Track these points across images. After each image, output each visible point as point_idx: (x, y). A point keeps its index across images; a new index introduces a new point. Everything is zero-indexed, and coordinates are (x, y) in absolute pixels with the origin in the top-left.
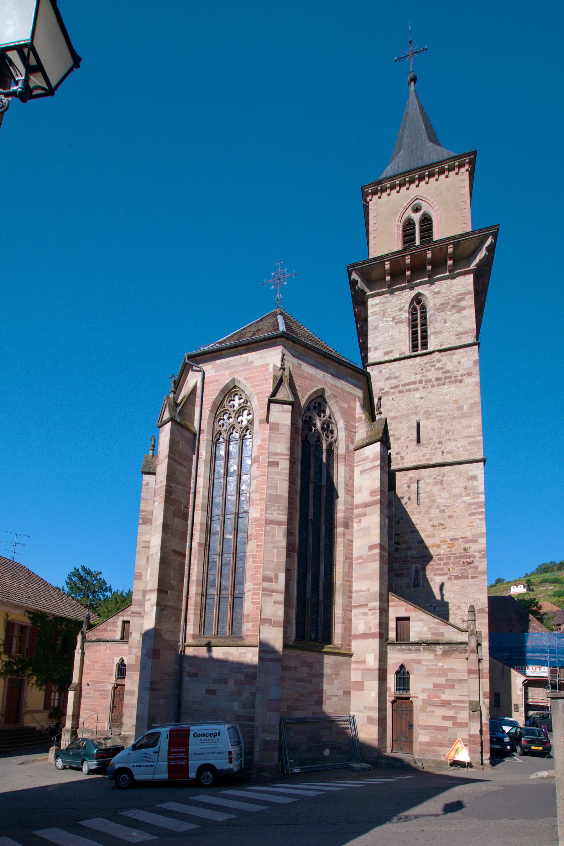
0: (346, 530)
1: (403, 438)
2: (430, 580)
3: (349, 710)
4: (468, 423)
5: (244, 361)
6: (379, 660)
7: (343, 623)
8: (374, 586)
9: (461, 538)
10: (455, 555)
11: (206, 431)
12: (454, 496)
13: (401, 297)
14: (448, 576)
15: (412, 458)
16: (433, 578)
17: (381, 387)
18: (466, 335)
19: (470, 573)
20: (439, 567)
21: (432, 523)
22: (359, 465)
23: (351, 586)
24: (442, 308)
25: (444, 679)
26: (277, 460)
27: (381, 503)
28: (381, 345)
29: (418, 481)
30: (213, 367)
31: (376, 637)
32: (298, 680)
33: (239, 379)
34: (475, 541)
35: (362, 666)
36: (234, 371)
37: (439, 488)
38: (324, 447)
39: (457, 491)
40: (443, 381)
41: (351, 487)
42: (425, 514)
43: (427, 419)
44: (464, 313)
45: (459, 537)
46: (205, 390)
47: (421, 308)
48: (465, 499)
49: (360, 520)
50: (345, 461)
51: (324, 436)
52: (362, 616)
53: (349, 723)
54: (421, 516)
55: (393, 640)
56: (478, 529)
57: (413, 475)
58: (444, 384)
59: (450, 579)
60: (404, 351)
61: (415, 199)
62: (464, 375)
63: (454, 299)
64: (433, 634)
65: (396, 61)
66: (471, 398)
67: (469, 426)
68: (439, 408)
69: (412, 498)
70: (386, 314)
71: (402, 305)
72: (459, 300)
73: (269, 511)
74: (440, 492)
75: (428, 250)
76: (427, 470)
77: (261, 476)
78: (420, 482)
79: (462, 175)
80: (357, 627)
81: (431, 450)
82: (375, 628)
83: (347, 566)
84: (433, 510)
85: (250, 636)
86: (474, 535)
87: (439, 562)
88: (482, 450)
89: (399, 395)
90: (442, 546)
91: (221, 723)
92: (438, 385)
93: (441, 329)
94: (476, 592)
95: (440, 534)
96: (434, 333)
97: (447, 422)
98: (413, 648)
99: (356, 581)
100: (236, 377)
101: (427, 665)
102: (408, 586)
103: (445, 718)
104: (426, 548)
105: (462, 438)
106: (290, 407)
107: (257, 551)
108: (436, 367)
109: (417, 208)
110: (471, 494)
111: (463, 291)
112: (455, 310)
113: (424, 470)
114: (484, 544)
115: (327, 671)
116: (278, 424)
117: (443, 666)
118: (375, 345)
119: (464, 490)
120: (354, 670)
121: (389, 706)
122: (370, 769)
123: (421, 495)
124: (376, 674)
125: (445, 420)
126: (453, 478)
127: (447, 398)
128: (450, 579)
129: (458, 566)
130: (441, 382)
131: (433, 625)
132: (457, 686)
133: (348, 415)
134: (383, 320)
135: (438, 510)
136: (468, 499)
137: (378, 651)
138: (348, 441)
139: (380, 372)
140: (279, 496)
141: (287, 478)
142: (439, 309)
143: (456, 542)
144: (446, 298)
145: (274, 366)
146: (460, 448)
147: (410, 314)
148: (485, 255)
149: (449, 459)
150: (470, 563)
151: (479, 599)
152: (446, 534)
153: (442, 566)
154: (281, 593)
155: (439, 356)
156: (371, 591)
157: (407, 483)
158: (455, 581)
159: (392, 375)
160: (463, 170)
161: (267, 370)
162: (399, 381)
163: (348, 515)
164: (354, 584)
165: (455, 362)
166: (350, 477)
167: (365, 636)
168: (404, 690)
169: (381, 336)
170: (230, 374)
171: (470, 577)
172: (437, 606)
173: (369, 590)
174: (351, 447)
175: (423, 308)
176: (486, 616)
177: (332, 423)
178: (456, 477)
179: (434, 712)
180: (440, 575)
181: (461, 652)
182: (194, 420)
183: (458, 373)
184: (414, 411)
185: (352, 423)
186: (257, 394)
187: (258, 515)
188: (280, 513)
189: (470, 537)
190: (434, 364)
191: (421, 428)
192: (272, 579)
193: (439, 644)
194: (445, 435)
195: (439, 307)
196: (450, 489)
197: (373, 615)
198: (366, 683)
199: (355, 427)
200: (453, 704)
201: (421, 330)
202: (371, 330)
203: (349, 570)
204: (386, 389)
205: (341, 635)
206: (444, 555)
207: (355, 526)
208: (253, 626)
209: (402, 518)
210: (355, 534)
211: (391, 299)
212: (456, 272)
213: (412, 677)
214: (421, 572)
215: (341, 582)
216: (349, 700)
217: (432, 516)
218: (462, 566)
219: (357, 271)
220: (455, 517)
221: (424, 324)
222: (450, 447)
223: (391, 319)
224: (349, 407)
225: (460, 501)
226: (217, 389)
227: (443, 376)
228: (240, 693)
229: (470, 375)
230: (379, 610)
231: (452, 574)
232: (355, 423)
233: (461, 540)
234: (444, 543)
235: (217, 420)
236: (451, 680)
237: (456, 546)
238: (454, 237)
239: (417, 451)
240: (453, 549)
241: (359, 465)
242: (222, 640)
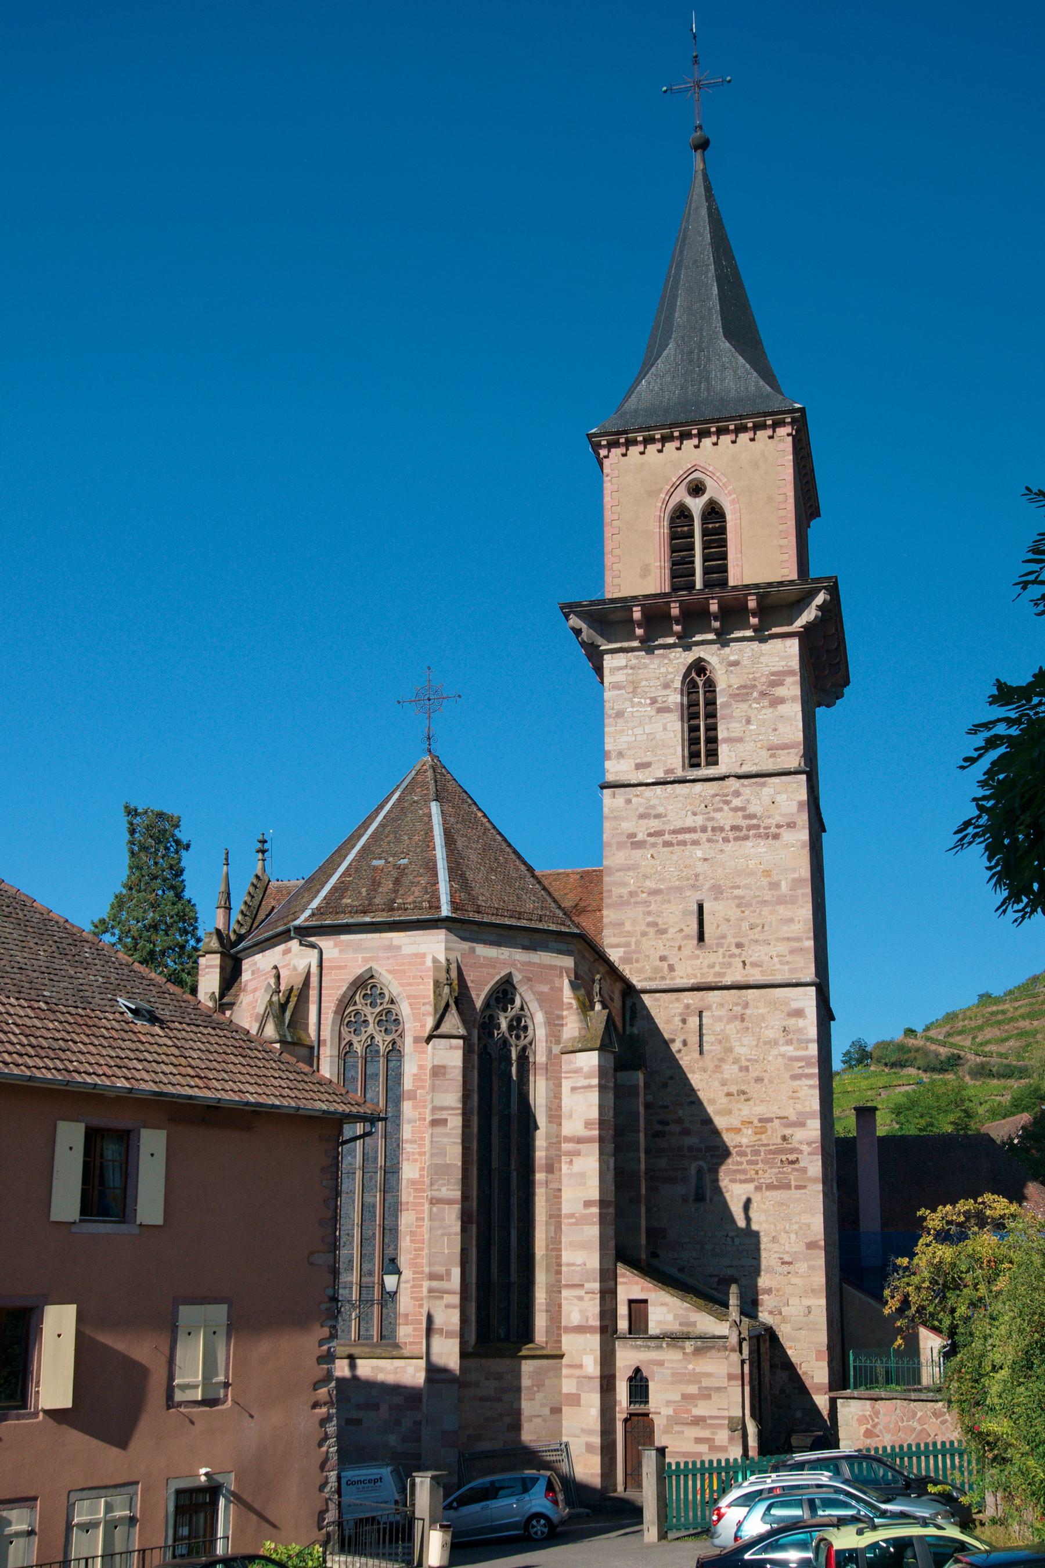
0: (550, 1176)
1: (671, 931)
2: (724, 1190)
3: (561, 1435)
4: (789, 914)
5: (386, 943)
6: (601, 1365)
7: (547, 1311)
8: (592, 1260)
9: (777, 1118)
10: (767, 1148)
11: (328, 1043)
12: (765, 1043)
13: (666, 661)
14: (756, 1183)
15: (689, 970)
16: (730, 1187)
17: (631, 831)
18: (786, 751)
19: (793, 1179)
20: (740, 1167)
21: (725, 1089)
22: (569, 1077)
23: (559, 1257)
24: (743, 694)
25: (696, 1387)
26: (444, 1117)
27: (601, 1140)
28: (629, 749)
29: (701, 1013)
30: (336, 945)
31: (596, 1333)
32: (482, 1399)
33: (380, 970)
34: (802, 1125)
35: (577, 1372)
36: (371, 957)
37: (738, 1028)
38: (514, 1056)
39: (770, 1034)
40: (744, 832)
41: (556, 1110)
42: (714, 1072)
43: (716, 899)
44: (782, 709)
45: (773, 1116)
46: (323, 978)
47: (704, 684)
48: (783, 1049)
49: (571, 1161)
50: (547, 1073)
51: (513, 1041)
52: (575, 1301)
53: (560, 1453)
54: (705, 1076)
55: (624, 1332)
56: (807, 1103)
57: (691, 1001)
58: (746, 838)
59: (758, 1188)
60: (672, 767)
61: (693, 469)
62: (783, 826)
63: (764, 680)
64: (681, 1324)
65: (665, 92)
66: (794, 870)
67: (791, 920)
68: (738, 881)
69: (689, 1042)
70: (639, 690)
71: (670, 677)
72: (774, 684)
73: (436, 1187)
74: (739, 1035)
75: (713, 598)
76: (716, 992)
77: (420, 1119)
78: (704, 1014)
79: (780, 440)
80: (569, 1316)
81: (724, 957)
82: (593, 1319)
83: (553, 1228)
84: (728, 1067)
85: (411, 1343)
86: (800, 1113)
87: (739, 1159)
88: (813, 965)
89: (665, 849)
90: (745, 1131)
91: (380, 1466)
92: (736, 839)
93: (741, 734)
94: (805, 1212)
95: (740, 1110)
96: (729, 740)
97: (751, 909)
98: (652, 1343)
99: (566, 1250)
100: (375, 966)
101: (672, 1368)
102: (685, 1200)
103: (698, 1440)
104: (716, 1133)
105: (778, 940)
106: (461, 1042)
107: (417, 1227)
108: (733, 805)
109: (697, 486)
110: (794, 1042)
111: (781, 669)
112: (766, 703)
113: (711, 993)
114: (816, 1130)
115: (526, 1382)
116: (444, 1067)
117: (694, 1369)
118: (619, 747)
119: (782, 1034)
120: (566, 1377)
121: (619, 1427)
122: (588, 1515)
123: (705, 1038)
124: (597, 1383)
125: (749, 905)
126: (762, 1011)
127: (752, 864)
128: (758, 1188)
129: (772, 1168)
130: (742, 834)
131: (681, 1312)
132: (714, 1396)
133: (551, 1003)
134: (632, 702)
135: (736, 1067)
136: (790, 1050)
137: (598, 1353)
138: (551, 1042)
139: (629, 801)
140: (448, 1166)
141: (459, 1141)
142: (738, 695)
143: (769, 1125)
144: (751, 676)
145: (435, 960)
146: (775, 959)
147: (685, 693)
148: (816, 617)
149: (756, 976)
150: (793, 1162)
151: (808, 1225)
152: (751, 1109)
153: (745, 1166)
154: (454, 1293)
155: (738, 785)
156: (588, 1266)
157: (681, 1014)
158: (768, 1193)
159: (651, 811)
160: (782, 431)
161: (424, 963)
162: (664, 823)
163: (553, 1152)
164: (563, 1253)
165: (767, 801)
166: (556, 1095)
167: (580, 1329)
168: (641, 1402)
169: (630, 732)
170: (365, 960)
171: (793, 1187)
172: (737, 1236)
173: (585, 1265)
174: (556, 1050)
175: (710, 686)
176: (822, 1253)
177: (525, 1016)
178: (768, 1009)
179: (682, 1432)
180: (742, 1182)
181: (719, 1350)
182: (307, 1024)
183: (770, 821)
184: (692, 882)
185: (557, 1012)
186: (409, 997)
187: (417, 1176)
188: (452, 1188)
189: (793, 1118)
190: (728, 798)
191: (705, 916)
192: (443, 1276)
193: (689, 1338)
194: (749, 932)
195: (737, 692)
196: (758, 1030)
197: (591, 1300)
198: (583, 1395)
199: (561, 1017)
200: (709, 1421)
201: (706, 725)
202: (610, 716)
203: (556, 1234)
204: (640, 837)
205: (544, 1329)
206: (747, 1147)
207: (565, 1168)
208: (415, 1330)
209: (672, 1078)
210: (564, 1180)
211: (647, 661)
212: (766, 633)
213: (651, 1384)
214: (707, 1176)
215: (543, 1252)
216: (560, 1421)
217: (726, 1076)
218: (779, 1168)
219: (579, 615)
220: (766, 1081)
221: (711, 715)
222: (757, 955)
223: (648, 701)
224: (551, 989)
225: (774, 1052)
226: (344, 980)
227: (744, 823)
228: (398, 1423)
229: (791, 827)
230: (599, 1295)
231: (762, 1181)
232: (562, 1010)
233: (777, 1122)
234: (747, 1126)
235: (346, 1022)
236: (706, 1388)
237: (769, 1132)
238: (757, 586)
239: (697, 957)
240: (763, 1136)
241: (569, 1077)
242: (367, 1350)
